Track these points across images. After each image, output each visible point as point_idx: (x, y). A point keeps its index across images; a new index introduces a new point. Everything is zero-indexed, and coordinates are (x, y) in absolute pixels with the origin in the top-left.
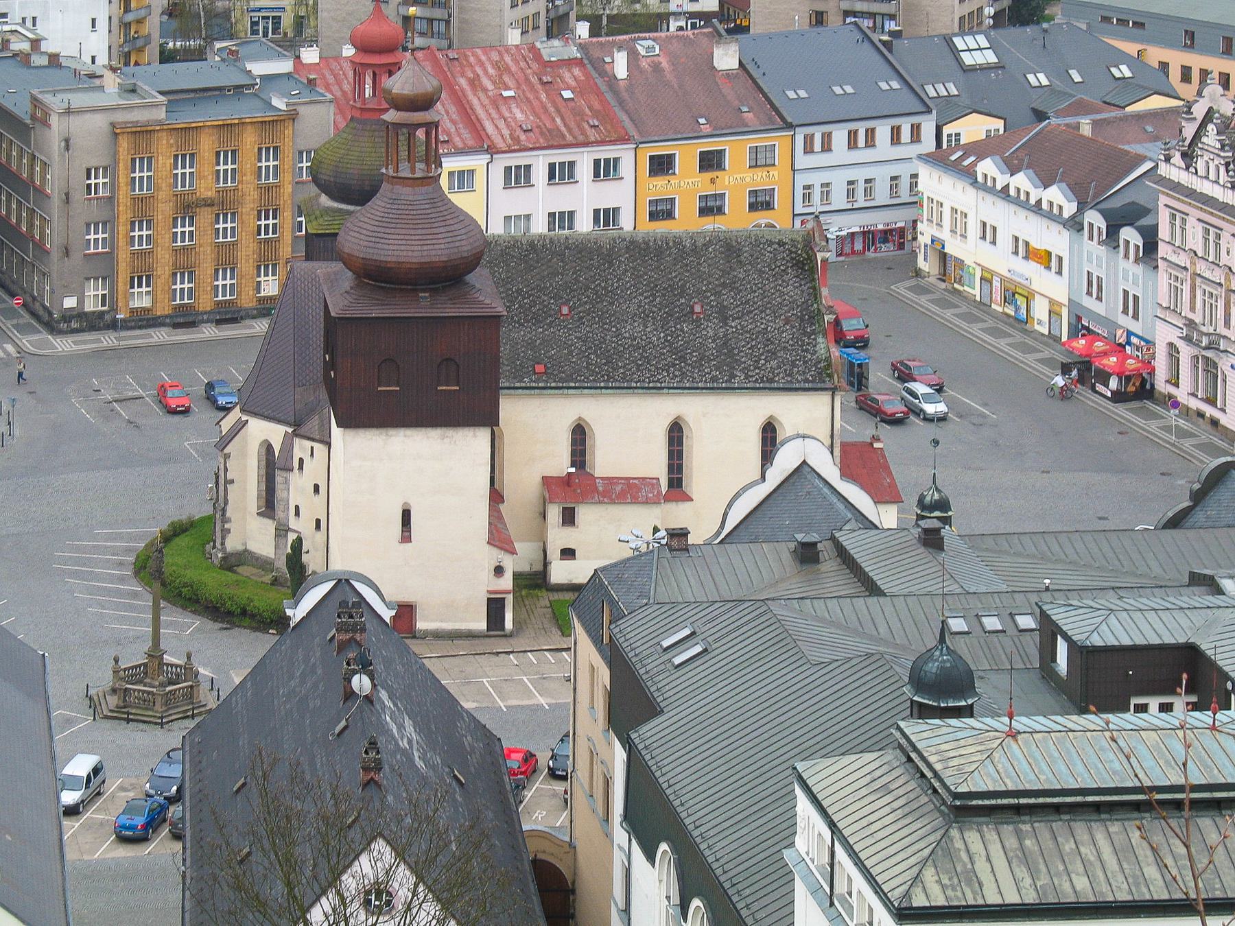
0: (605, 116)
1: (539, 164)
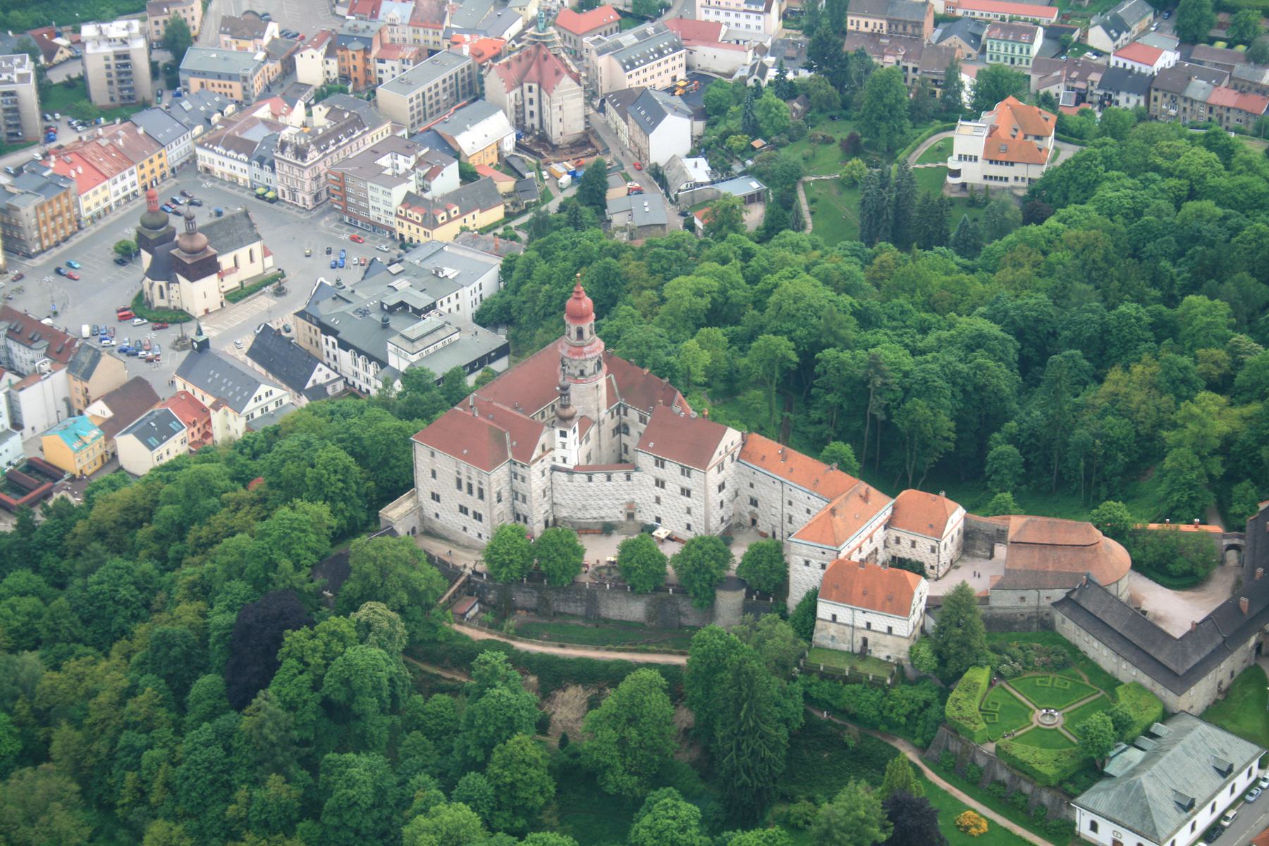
0: (126, 158)
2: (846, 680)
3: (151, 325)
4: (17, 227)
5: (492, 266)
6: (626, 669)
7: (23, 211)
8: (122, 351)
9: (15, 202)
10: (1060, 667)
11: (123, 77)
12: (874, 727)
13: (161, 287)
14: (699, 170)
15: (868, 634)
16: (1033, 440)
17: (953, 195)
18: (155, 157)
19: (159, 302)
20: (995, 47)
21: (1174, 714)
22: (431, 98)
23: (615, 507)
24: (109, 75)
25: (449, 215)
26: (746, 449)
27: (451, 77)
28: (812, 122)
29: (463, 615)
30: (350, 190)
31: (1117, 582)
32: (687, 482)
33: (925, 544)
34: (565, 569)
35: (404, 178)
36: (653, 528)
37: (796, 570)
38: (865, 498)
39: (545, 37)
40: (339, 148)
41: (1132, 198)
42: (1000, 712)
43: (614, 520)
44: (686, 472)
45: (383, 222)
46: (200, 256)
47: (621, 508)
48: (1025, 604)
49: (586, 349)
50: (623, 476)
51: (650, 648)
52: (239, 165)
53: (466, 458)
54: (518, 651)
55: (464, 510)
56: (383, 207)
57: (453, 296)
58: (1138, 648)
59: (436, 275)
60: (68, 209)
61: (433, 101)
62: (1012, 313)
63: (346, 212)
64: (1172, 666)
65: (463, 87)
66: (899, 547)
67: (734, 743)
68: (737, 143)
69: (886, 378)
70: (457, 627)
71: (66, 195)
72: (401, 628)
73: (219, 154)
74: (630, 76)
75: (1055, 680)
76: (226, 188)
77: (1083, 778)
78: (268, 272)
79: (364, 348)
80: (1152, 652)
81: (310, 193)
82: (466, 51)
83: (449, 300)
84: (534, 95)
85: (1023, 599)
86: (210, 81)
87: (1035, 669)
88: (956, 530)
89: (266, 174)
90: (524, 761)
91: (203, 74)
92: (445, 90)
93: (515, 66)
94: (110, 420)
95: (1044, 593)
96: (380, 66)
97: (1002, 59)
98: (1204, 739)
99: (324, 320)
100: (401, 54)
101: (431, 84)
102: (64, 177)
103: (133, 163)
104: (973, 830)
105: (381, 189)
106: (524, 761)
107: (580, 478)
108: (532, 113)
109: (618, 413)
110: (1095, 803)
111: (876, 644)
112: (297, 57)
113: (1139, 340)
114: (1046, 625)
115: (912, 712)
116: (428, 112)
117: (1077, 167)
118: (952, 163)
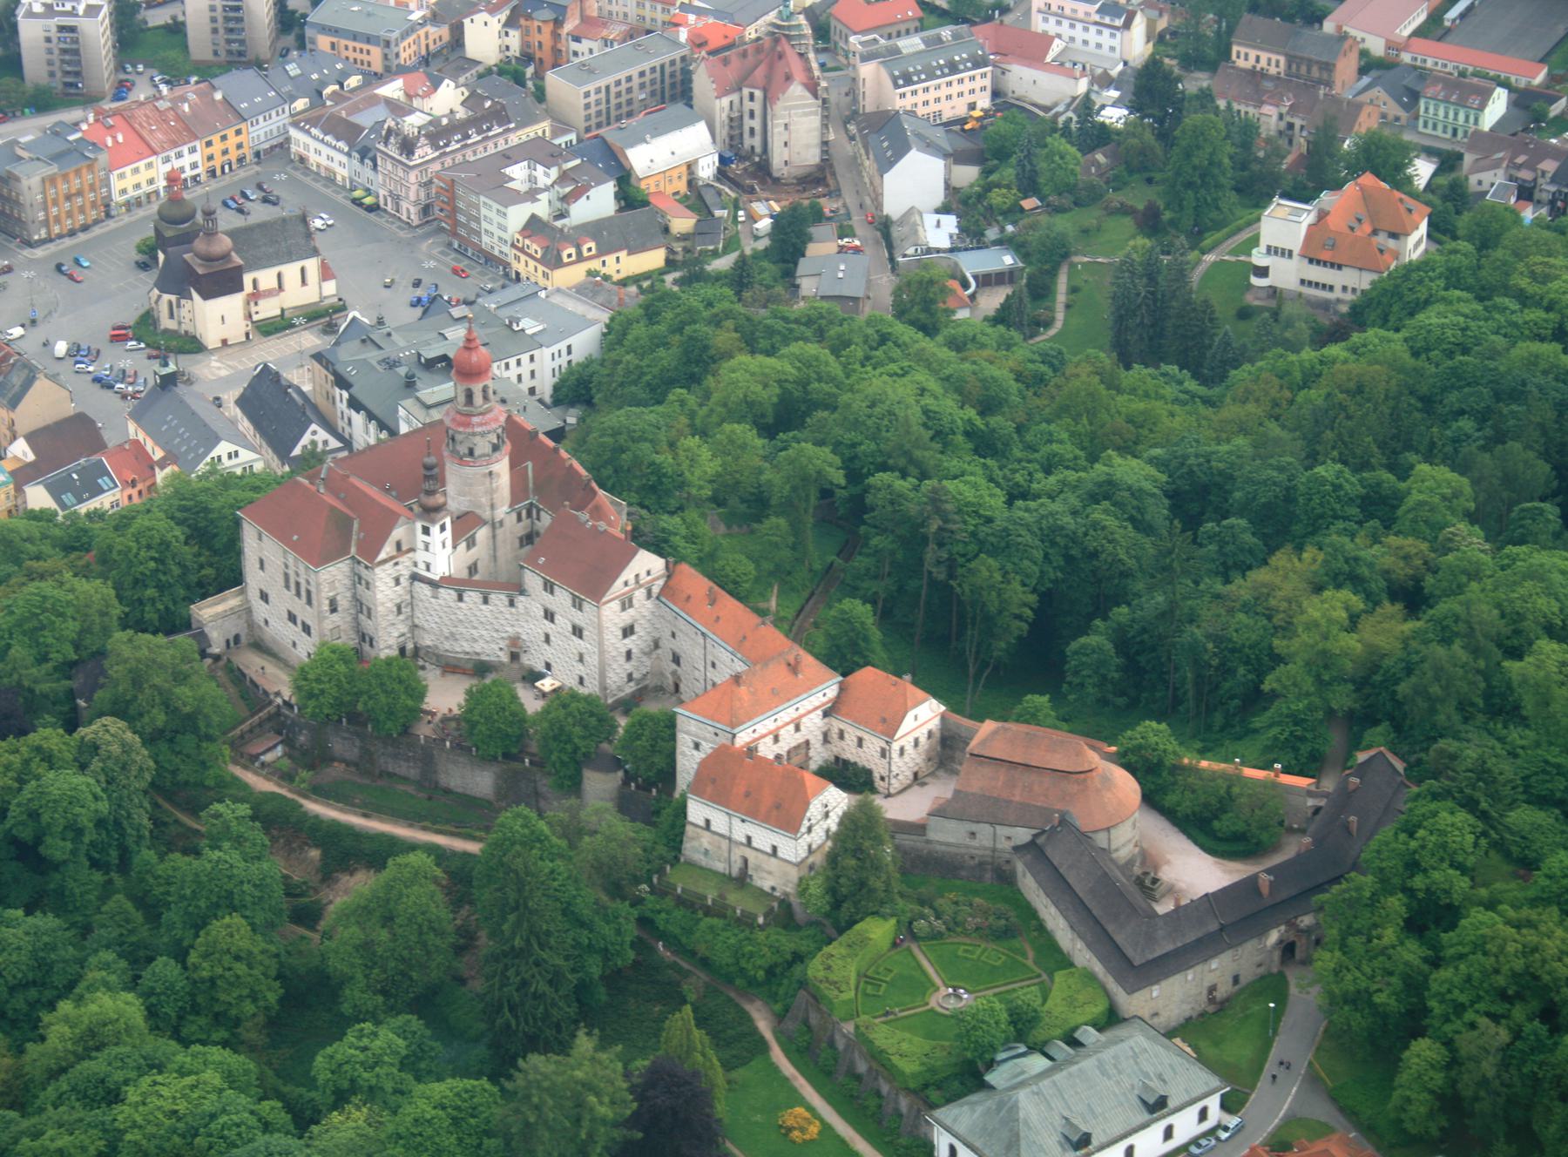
0: (188, 129)
1: (172, 154)
2: (708, 912)
3: (149, 351)
4: (17, 203)
5: (592, 323)
6: (395, 847)
7: (25, 183)
8: (97, 380)
9: (17, 170)
10: (1004, 934)
11: (231, 25)
12: (729, 980)
13: (170, 303)
14: (940, 232)
15: (748, 853)
16: (1146, 637)
17: (1257, 303)
18: (230, 132)
19: (166, 323)
20: (1431, 110)
21: (1125, 1020)
22: (619, 95)
23: (494, 640)
24: (214, 20)
25: (579, 253)
26: (671, 583)
27: (653, 70)
28: (1118, 184)
29: (256, 757)
30: (461, 205)
31: (1108, 829)
32: (580, 618)
33: (873, 744)
34: (392, 713)
35: (532, 195)
36: (541, 676)
37: (684, 754)
38: (794, 668)
39: (789, 28)
40: (466, 146)
41: (1464, 330)
42: (891, 984)
43: (492, 659)
44: (578, 604)
45: (496, 253)
46: (218, 266)
47: (503, 644)
48: (975, 843)
49: (475, 420)
50: (506, 600)
51: (478, 834)
52: (339, 157)
53: (294, 547)
54: (305, 814)
55: (292, 618)
56: (498, 233)
57: (525, 358)
58: (1097, 922)
59: (510, 326)
60: (92, 188)
61: (623, 99)
62: (1192, 461)
63: (455, 234)
64: (1129, 952)
65: (673, 85)
66: (843, 744)
67: (501, 966)
68: (1000, 199)
69: (946, 521)
70: (237, 771)
71: (90, 168)
72: (142, 755)
73: (315, 138)
74: (903, 95)
75: (992, 954)
76: (318, 186)
77: (956, 1084)
78: (327, 302)
79: (376, 411)
80: (1110, 928)
81: (416, 203)
82: (683, 35)
83: (519, 363)
84: (757, 106)
85: (973, 834)
86: (343, 42)
87: (966, 934)
88: (924, 730)
89: (367, 172)
90: (228, 951)
91: (334, 31)
92: (642, 86)
93: (736, 63)
94: (30, 464)
95: (1002, 831)
96: (574, 46)
97: (1440, 127)
98: (1135, 1056)
99: (339, 368)
100: (605, 33)
101: (622, 76)
102: (94, 144)
103: (196, 138)
104: (796, 1134)
105: (495, 206)
106: (228, 951)
107: (447, 595)
108: (752, 131)
109: (529, 515)
110: (955, 1120)
111: (758, 868)
112: (467, 22)
113: (1336, 517)
114: (1006, 878)
115: (776, 965)
116: (613, 113)
117: (1406, 277)
118: (1258, 258)
